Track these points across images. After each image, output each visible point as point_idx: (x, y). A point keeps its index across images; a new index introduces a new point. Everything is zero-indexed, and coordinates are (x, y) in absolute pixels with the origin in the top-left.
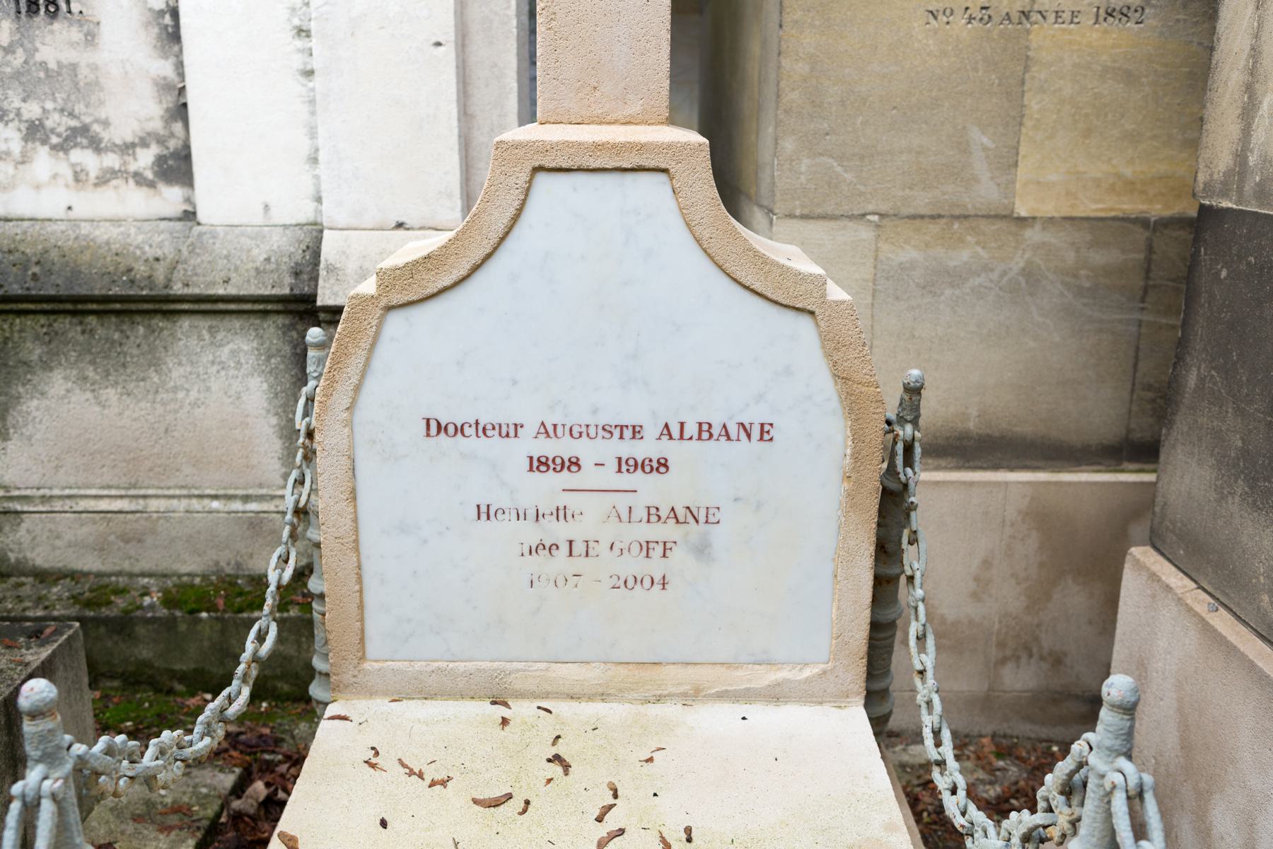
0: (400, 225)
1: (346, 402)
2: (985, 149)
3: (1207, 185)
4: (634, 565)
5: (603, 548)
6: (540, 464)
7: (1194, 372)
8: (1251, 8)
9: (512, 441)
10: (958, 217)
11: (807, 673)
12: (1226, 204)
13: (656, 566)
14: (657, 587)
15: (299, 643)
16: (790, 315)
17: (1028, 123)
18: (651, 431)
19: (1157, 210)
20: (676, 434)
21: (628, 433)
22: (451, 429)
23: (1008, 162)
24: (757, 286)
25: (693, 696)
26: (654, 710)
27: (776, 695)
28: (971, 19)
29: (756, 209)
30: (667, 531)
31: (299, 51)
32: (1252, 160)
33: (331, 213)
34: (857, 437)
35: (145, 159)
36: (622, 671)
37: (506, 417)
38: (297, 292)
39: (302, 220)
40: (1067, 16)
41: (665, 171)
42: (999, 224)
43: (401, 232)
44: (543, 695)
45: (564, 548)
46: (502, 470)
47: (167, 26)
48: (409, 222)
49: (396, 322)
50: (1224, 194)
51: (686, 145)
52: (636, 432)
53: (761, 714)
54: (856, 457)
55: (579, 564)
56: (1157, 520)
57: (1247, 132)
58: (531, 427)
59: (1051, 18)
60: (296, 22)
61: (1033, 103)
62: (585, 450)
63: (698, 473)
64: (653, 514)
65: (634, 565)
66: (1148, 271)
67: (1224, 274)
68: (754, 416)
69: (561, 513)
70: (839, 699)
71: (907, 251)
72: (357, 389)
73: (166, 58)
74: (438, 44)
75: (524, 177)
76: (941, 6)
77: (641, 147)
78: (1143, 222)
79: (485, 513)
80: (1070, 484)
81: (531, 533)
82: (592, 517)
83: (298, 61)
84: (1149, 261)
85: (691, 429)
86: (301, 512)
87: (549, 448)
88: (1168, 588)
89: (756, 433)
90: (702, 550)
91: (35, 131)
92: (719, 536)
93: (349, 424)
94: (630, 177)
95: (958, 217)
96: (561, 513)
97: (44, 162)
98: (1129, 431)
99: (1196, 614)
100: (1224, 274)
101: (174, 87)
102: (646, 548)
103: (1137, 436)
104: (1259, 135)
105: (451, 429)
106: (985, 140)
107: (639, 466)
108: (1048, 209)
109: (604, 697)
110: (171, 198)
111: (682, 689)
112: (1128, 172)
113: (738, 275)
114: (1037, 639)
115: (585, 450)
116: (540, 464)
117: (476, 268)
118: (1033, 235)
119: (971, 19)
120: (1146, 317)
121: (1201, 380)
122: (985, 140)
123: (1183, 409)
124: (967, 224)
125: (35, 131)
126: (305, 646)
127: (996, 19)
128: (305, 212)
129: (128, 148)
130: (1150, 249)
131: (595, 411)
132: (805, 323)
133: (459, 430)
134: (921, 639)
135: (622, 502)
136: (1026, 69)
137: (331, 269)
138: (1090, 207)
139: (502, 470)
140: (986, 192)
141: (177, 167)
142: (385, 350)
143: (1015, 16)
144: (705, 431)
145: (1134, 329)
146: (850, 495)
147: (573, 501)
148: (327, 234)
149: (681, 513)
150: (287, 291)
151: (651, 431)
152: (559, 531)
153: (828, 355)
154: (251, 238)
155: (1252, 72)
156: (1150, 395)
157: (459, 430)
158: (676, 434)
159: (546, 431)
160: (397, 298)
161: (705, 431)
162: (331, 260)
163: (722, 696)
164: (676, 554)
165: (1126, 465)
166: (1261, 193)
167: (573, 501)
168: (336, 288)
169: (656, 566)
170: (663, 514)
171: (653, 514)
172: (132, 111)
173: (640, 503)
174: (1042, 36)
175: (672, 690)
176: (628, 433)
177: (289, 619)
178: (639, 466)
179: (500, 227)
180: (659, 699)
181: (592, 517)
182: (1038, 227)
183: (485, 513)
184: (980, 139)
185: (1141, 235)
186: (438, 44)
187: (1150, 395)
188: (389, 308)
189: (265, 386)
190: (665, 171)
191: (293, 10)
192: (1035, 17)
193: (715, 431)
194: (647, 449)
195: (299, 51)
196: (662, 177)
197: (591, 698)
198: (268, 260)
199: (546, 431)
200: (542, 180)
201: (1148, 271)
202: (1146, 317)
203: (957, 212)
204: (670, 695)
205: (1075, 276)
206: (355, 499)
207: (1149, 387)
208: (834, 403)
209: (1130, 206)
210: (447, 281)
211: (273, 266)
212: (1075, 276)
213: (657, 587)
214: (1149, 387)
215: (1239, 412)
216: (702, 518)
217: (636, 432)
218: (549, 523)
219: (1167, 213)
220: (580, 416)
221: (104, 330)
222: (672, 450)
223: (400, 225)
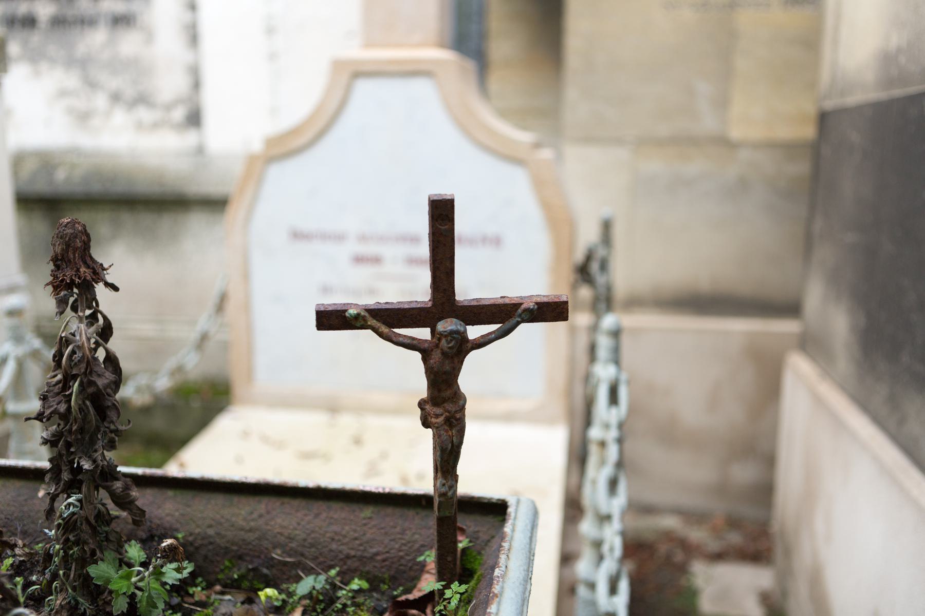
6: (359, 260)
23: (722, 103)
35: (179, 114)
44: (361, 409)
70: (550, 421)
71: (655, 165)
86: (30, 22)
91: (116, 98)
97: (120, 117)
110: (190, 139)
116: (359, 260)
118: (744, 154)
125: (116, 98)
129: (169, 107)
140: (708, 123)
141: (194, 119)
172: (170, 85)
189: (485, 558)
200: (364, 89)
221: (146, 218)
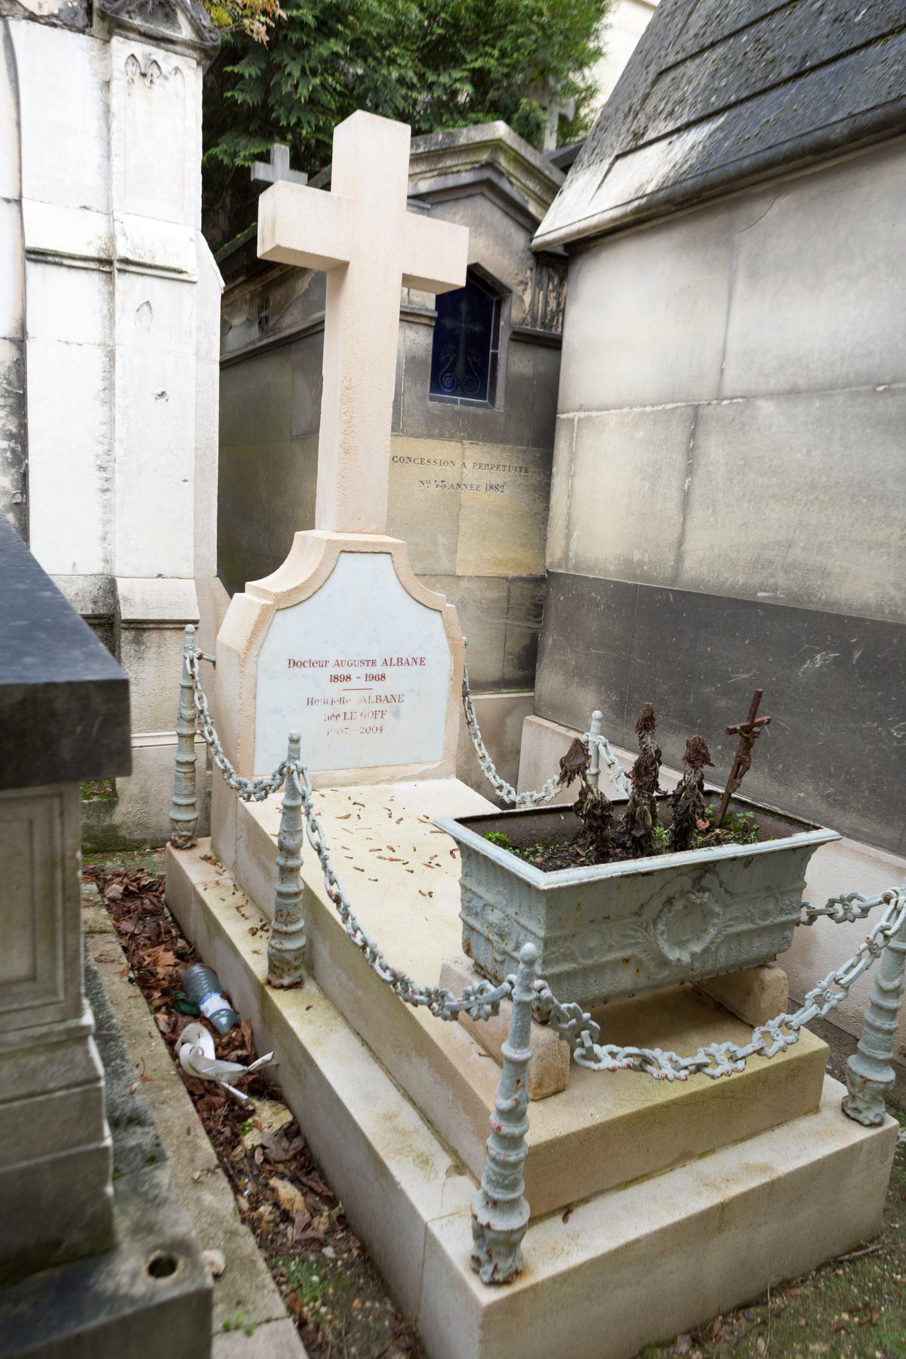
0: (160, 576)
1: (256, 653)
2: (444, 544)
3: (551, 564)
4: (370, 722)
5: (357, 716)
6: (335, 678)
7: (551, 638)
8: (566, 497)
9: (324, 668)
10: (433, 575)
11: (435, 766)
12: (560, 571)
13: (378, 723)
14: (379, 731)
15: (98, 817)
16: (433, 612)
17: (461, 533)
18: (379, 662)
19: (512, 574)
20: (389, 663)
21: (370, 663)
22: (299, 664)
23: (453, 550)
24: (421, 601)
25: (392, 780)
26: (379, 786)
27: (423, 777)
28: (437, 486)
29: (689, 564)
30: (383, 706)
31: (99, 478)
32: (571, 555)
33: (119, 569)
34: (456, 662)
36: (363, 771)
37: (322, 658)
38: (96, 613)
39: (95, 572)
40: (475, 487)
41: (390, 554)
42: (451, 579)
43: (160, 579)
45: (342, 716)
46: (318, 682)
47: (7, 458)
48: (165, 574)
49: (280, 614)
50: (560, 567)
51: (398, 544)
52: (374, 663)
53: (421, 784)
54: (455, 670)
55: (348, 723)
56: (536, 703)
57: (568, 544)
58: (332, 662)
59: (469, 487)
60: (99, 462)
61: (462, 524)
62: (353, 671)
63: (398, 680)
64: (378, 699)
65: (370, 722)
66: (509, 601)
67: (562, 598)
68: (418, 655)
69: (342, 700)
72: (261, 646)
73: (6, 476)
74: (186, 481)
75: (337, 554)
76: (425, 479)
77: (382, 544)
78: (506, 579)
79: (310, 702)
80: (482, 700)
81: (329, 710)
82: (354, 702)
83: (100, 484)
84: (509, 596)
85: (395, 661)
87: (340, 671)
88: (547, 728)
89: (419, 662)
90: (397, 714)
92: (403, 706)
93: (256, 663)
94: (377, 555)
95: (433, 575)
96: (342, 700)
98: (504, 674)
99: (562, 734)
100: (562, 598)
101: (10, 493)
102: (375, 714)
103: (506, 676)
104: (573, 545)
105: (299, 664)
106: (444, 540)
107: (374, 678)
108: (470, 572)
109: (355, 784)
111: (388, 777)
112: (500, 556)
113: (413, 593)
114: (470, 777)
115: (353, 671)
116: (335, 678)
117: (315, 592)
118: (464, 584)
119: (437, 486)
120: (509, 622)
121: (555, 641)
122: (444, 540)
123: (546, 654)
124: (437, 578)
126: (102, 819)
127: (447, 487)
128: (98, 567)
130: (509, 591)
131: (358, 654)
132: (438, 615)
133: (303, 664)
134: (480, 745)
135: (366, 694)
136: (460, 509)
137: (126, 599)
138: (486, 572)
139: (318, 682)
140: (444, 564)
142: (274, 629)
143: (455, 486)
144: (400, 661)
145: (504, 627)
146: (453, 687)
147: (347, 695)
148: (119, 582)
149: (389, 698)
150: (90, 612)
151: (379, 662)
152: (340, 708)
153: (446, 629)
154: (65, 582)
155: (568, 522)
156: (511, 657)
157: (303, 664)
158: (389, 663)
159: (338, 664)
160: (282, 606)
161: (400, 661)
162: (125, 595)
163: (403, 779)
164: (387, 716)
165: (503, 690)
166: (576, 567)
167: (347, 695)
168: (131, 610)
169: (378, 723)
170: (382, 698)
171: (378, 699)
173: (374, 694)
174: (466, 495)
175: (383, 778)
176: (370, 663)
177: (94, 803)
178: (374, 678)
179: (327, 576)
180: (377, 783)
181: (354, 702)
182: (466, 580)
183: (310, 702)
184: (442, 540)
185: (505, 585)
186: (186, 481)
187: (511, 657)
188: (278, 610)
190: (390, 554)
191: (98, 456)
192: (463, 487)
193: (404, 661)
194: (377, 670)
195: (99, 478)
196: (389, 556)
197: (350, 785)
198: (77, 594)
199: (338, 664)
201: (509, 601)
202: (509, 622)
203: (433, 573)
204: (382, 781)
205: (481, 603)
206: (255, 698)
207: (510, 654)
208: (447, 649)
209: (502, 572)
210: (304, 598)
211: (80, 598)
212: (481, 603)
213: (379, 731)
214: (510, 654)
215: (573, 651)
216: (397, 700)
217: (374, 663)
218: (337, 705)
219: (515, 575)
220: (352, 657)
222: (387, 670)
223: (160, 576)
